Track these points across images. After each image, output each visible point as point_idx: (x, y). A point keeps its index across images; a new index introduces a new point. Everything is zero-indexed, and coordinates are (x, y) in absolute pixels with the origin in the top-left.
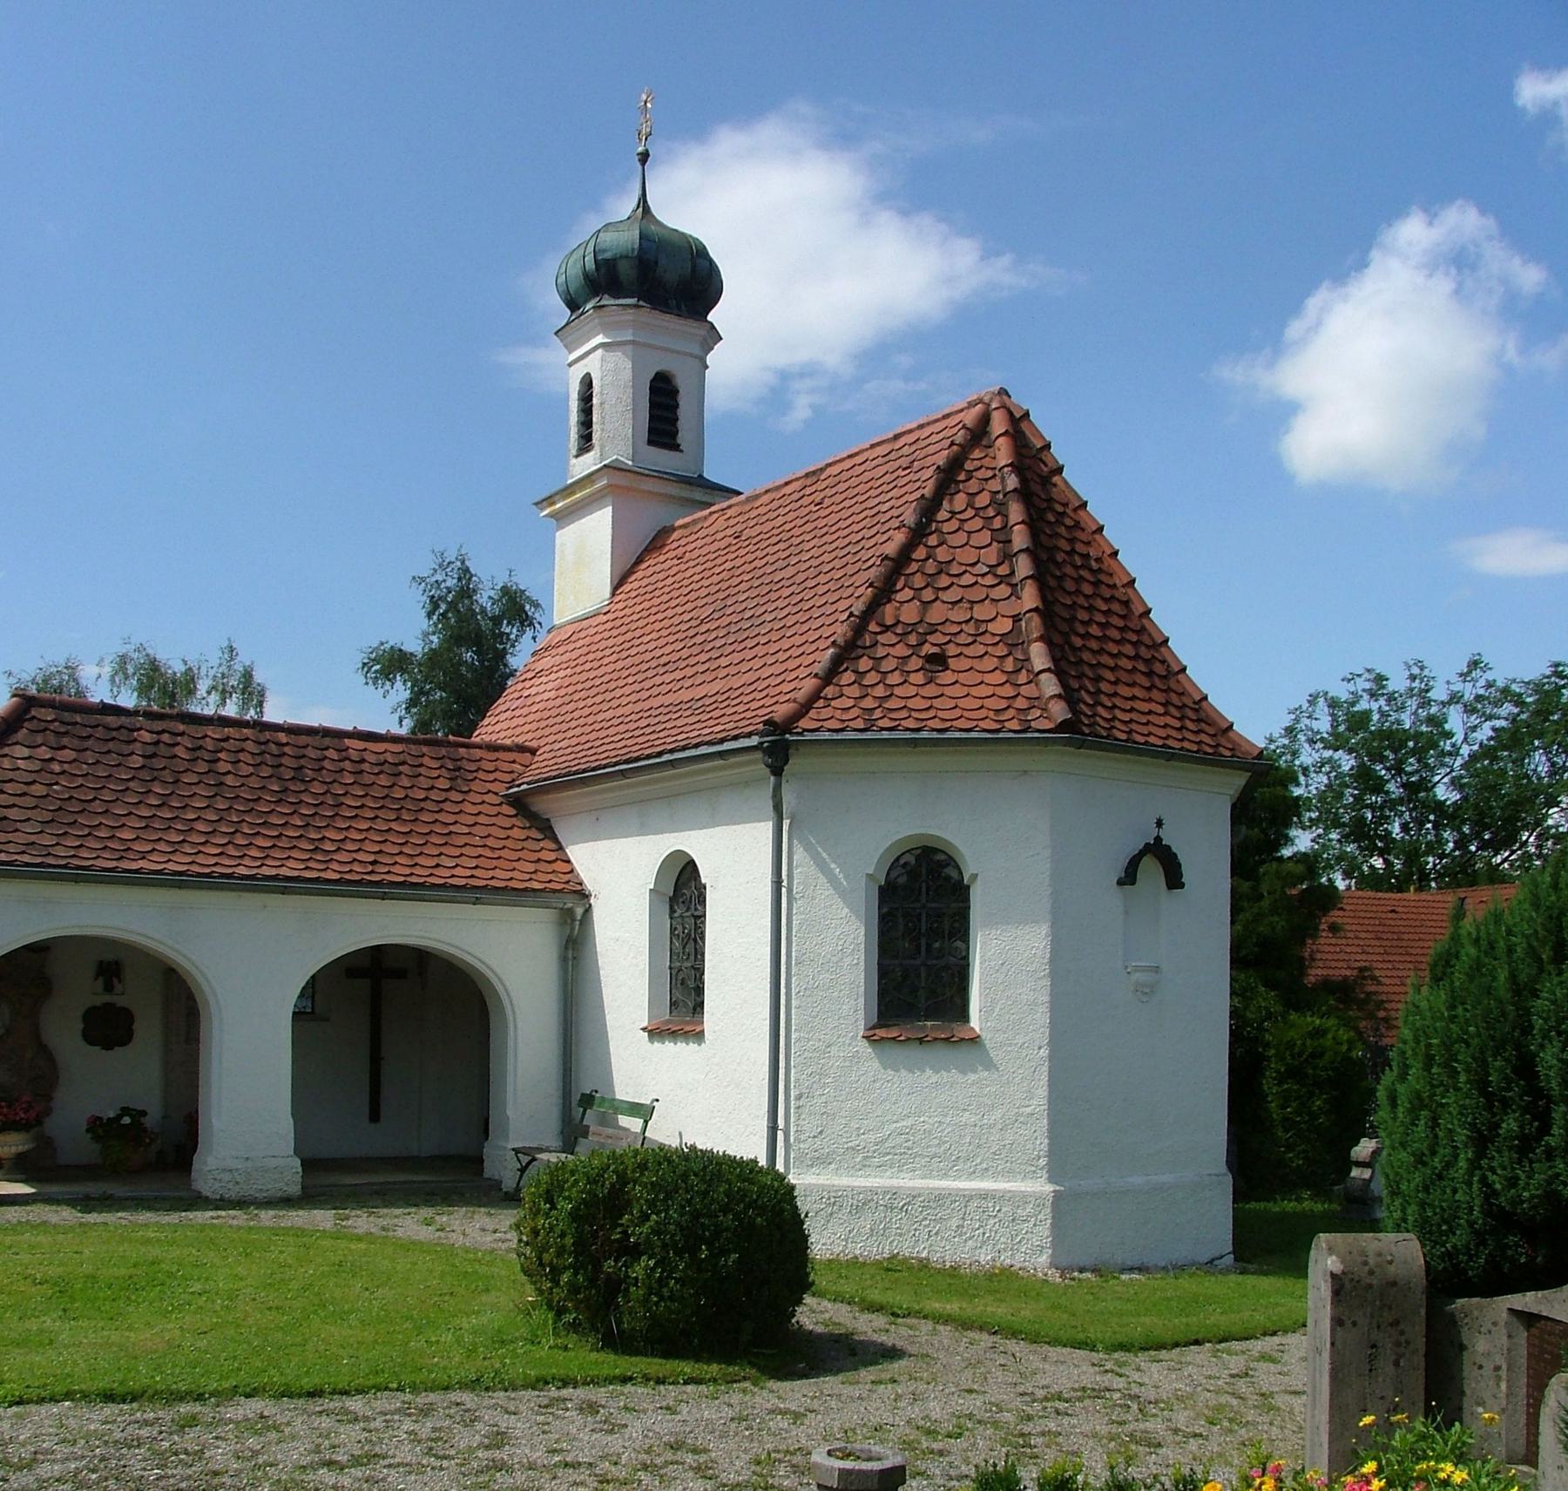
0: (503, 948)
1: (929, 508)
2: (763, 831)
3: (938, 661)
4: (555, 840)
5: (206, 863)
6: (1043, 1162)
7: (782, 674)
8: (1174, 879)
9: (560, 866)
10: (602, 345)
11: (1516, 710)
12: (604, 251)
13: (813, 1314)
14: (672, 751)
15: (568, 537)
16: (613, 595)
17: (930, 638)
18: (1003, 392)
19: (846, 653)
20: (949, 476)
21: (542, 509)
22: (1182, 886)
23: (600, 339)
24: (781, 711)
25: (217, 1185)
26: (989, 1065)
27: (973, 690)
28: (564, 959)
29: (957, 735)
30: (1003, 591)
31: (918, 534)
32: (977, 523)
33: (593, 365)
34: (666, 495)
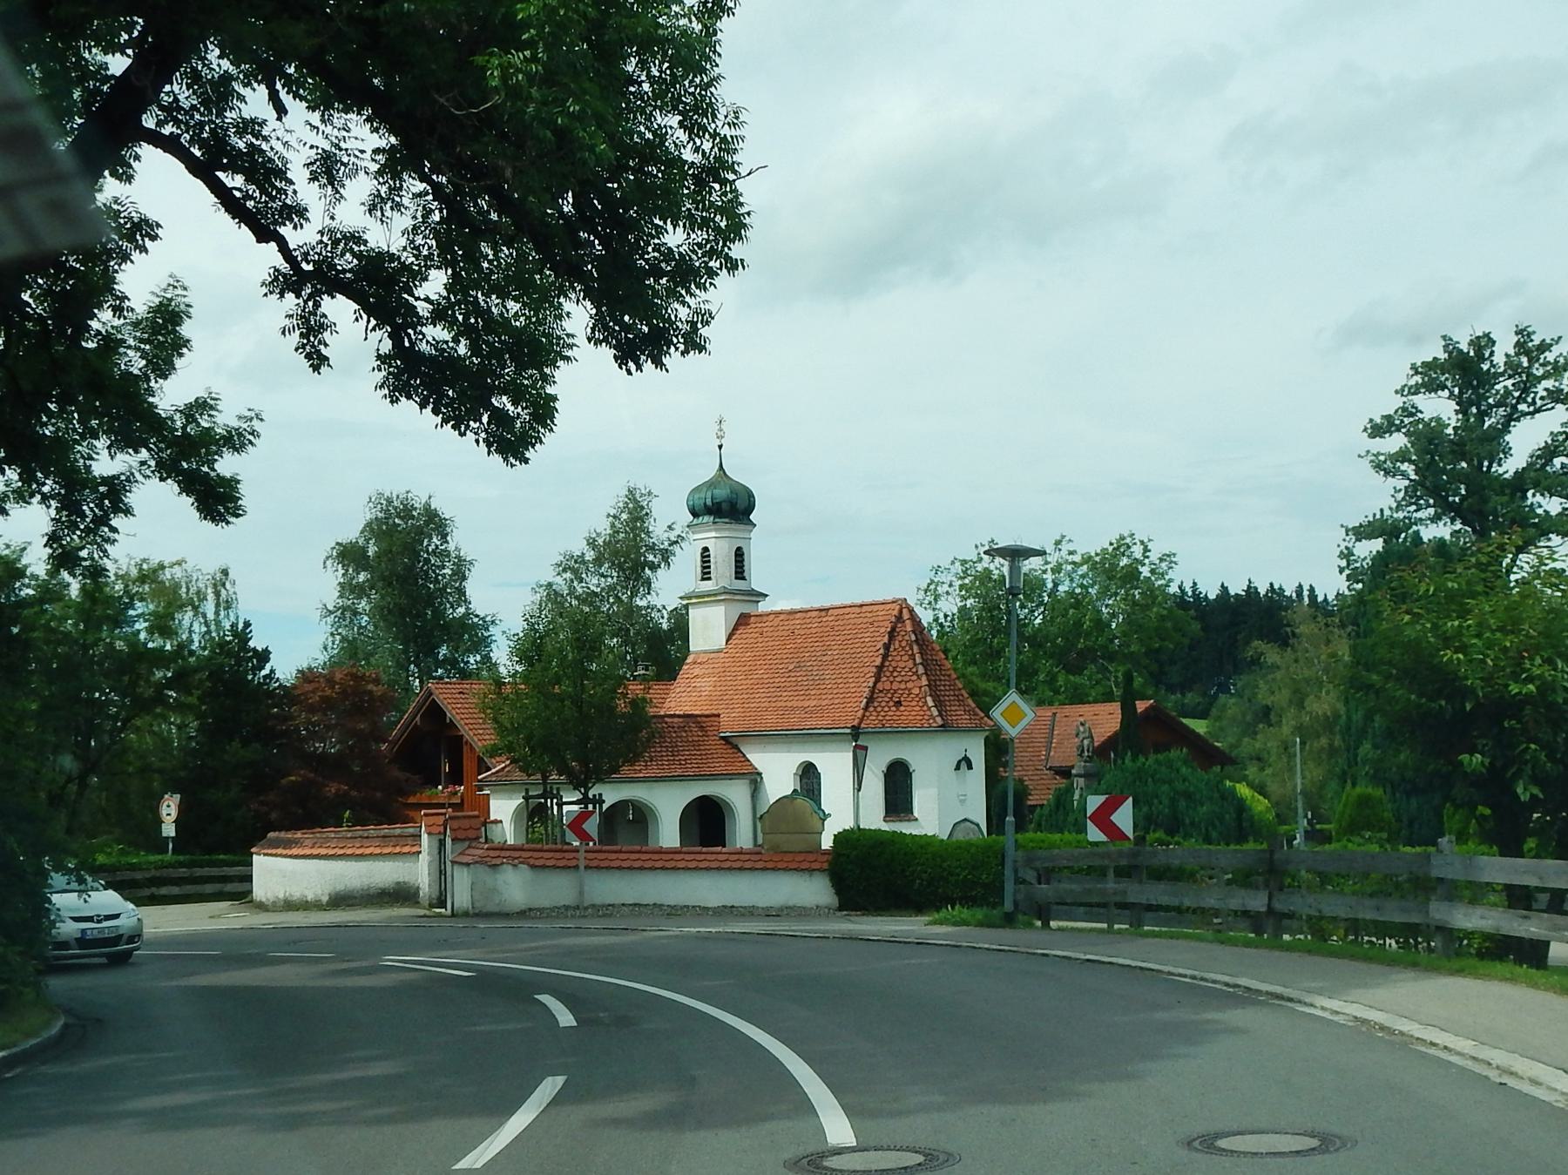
1: (887, 647)
3: (898, 704)
7: (852, 712)
8: (970, 767)
11: (605, 807)
19: (870, 700)
20: (892, 634)
24: (856, 723)
27: (910, 714)
31: (885, 657)
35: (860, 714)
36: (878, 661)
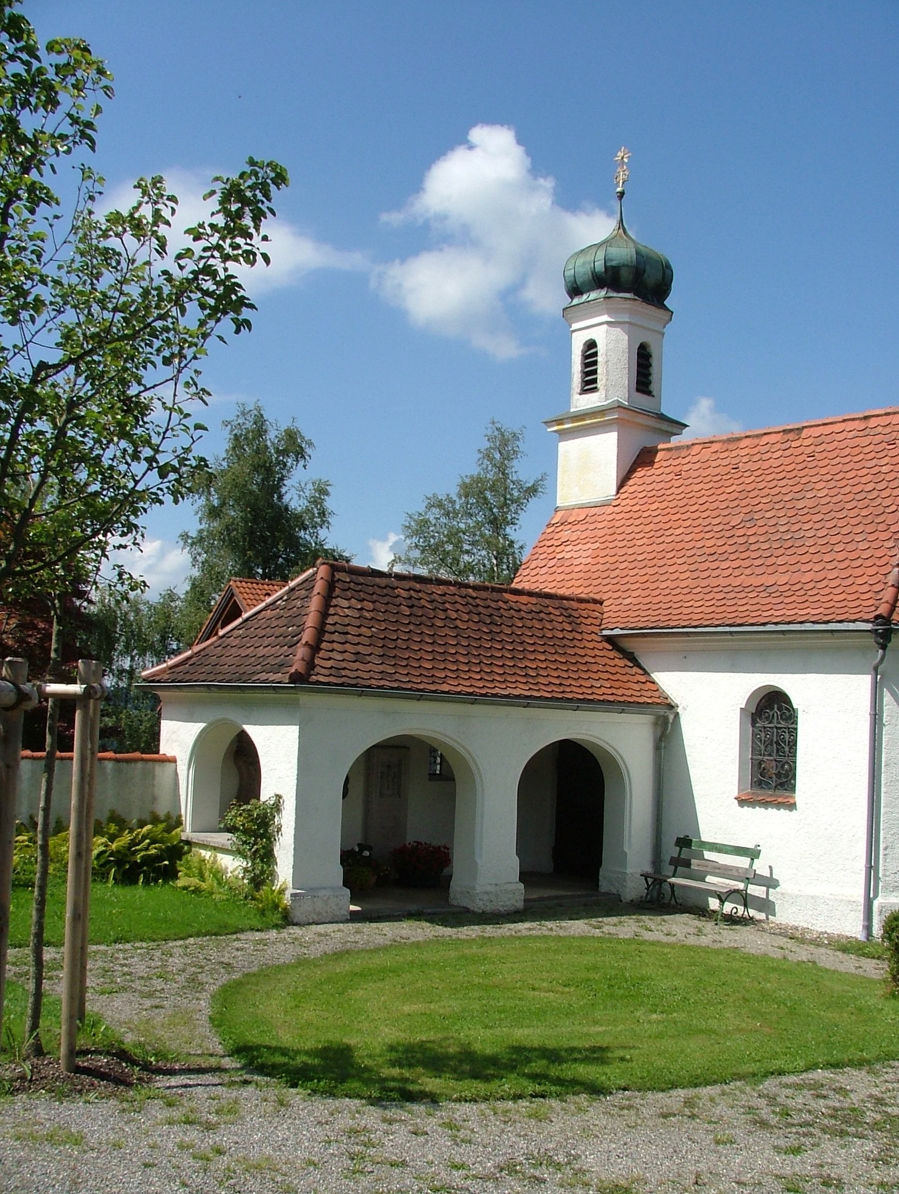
0: (624, 740)
2: (864, 682)
4: (639, 666)
10: (607, 323)
12: (612, 260)
14: (776, 624)
16: (618, 493)
21: (550, 427)
25: (481, 903)
28: (658, 748)
33: (600, 335)
34: (659, 429)
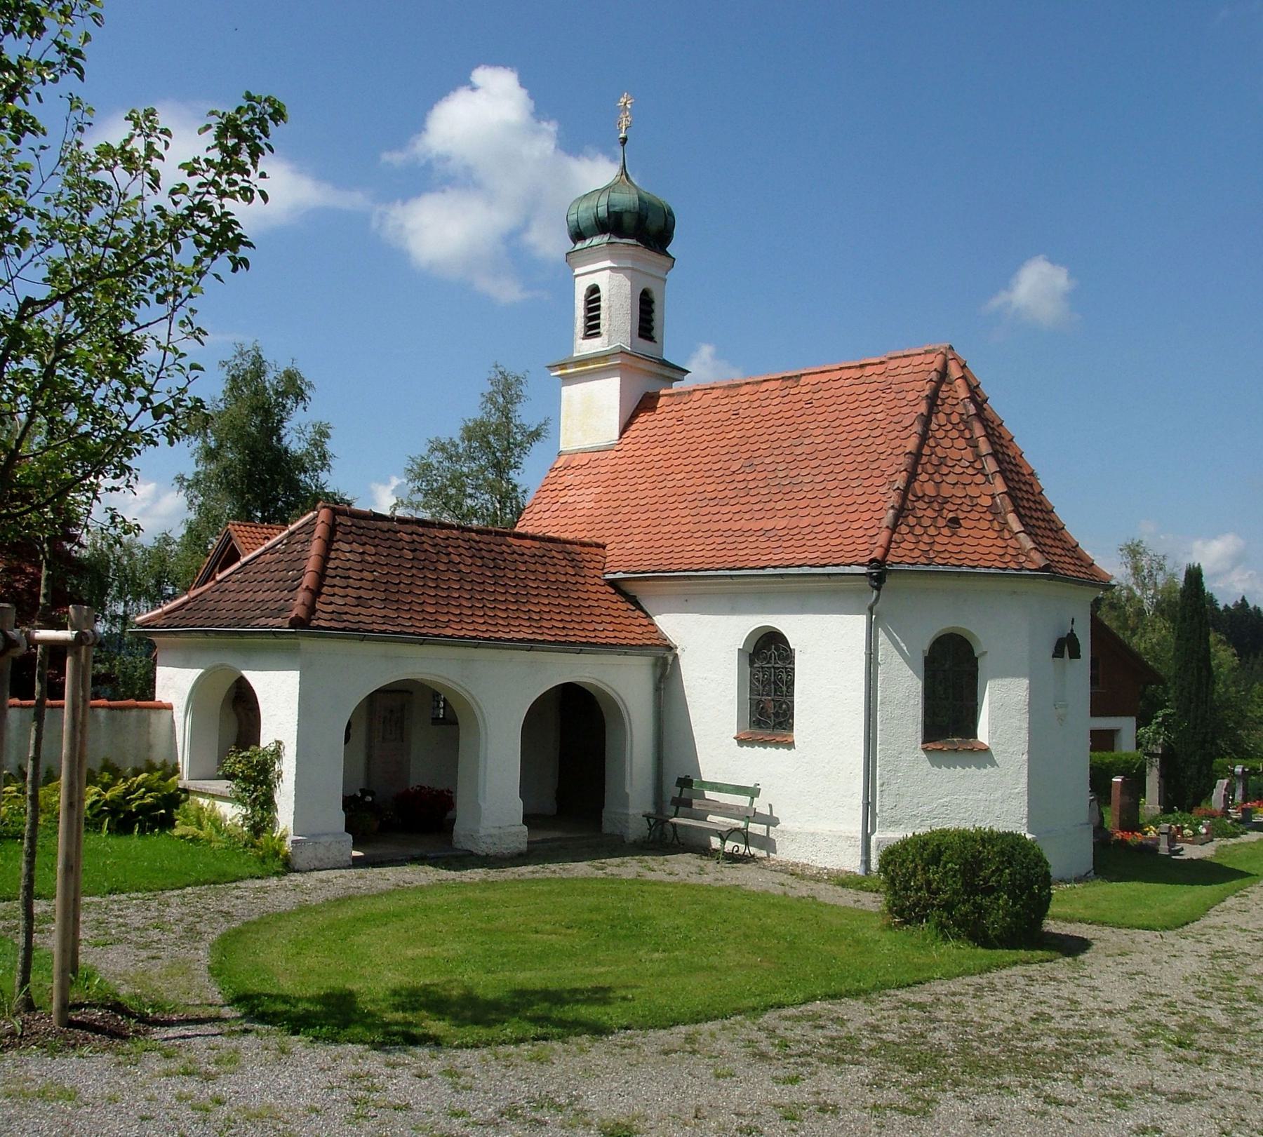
0: (625, 681)
1: (926, 420)
2: (858, 623)
5: (482, 630)
6: (1025, 821)
7: (863, 528)
8: (1075, 654)
9: (651, 628)
13: (1051, 926)
14: (775, 567)
15: (573, 394)
17: (946, 506)
18: (951, 348)
19: (901, 512)
20: (933, 401)
22: (1079, 657)
23: (608, 263)
24: (877, 553)
26: (993, 763)
29: (983, 570)
30: (979, 479)
31: (924, 438)
32: (955, 434)
35: (882, 538)
36: (912, 444)
